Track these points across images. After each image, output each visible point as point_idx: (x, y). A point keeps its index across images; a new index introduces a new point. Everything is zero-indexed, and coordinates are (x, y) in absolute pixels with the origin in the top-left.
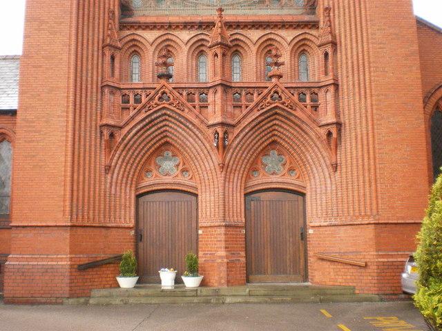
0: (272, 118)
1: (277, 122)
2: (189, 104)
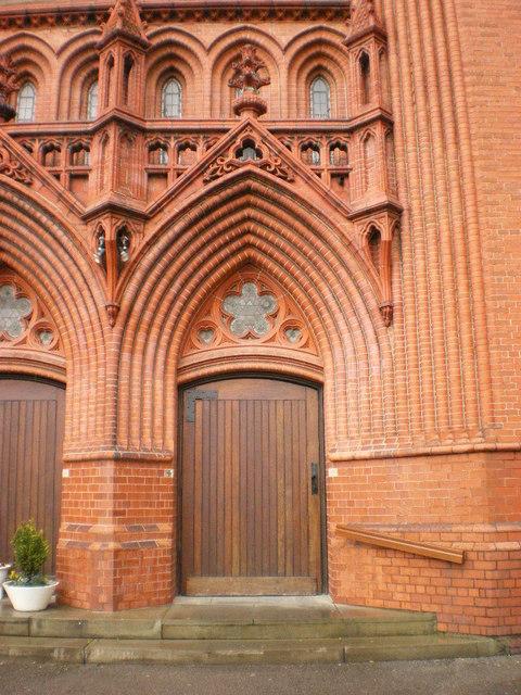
0: (239, 201)
1: (252, 212)
2: (44, 171)
